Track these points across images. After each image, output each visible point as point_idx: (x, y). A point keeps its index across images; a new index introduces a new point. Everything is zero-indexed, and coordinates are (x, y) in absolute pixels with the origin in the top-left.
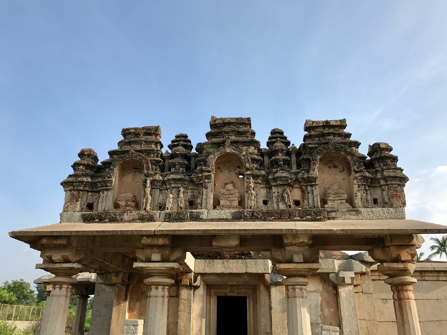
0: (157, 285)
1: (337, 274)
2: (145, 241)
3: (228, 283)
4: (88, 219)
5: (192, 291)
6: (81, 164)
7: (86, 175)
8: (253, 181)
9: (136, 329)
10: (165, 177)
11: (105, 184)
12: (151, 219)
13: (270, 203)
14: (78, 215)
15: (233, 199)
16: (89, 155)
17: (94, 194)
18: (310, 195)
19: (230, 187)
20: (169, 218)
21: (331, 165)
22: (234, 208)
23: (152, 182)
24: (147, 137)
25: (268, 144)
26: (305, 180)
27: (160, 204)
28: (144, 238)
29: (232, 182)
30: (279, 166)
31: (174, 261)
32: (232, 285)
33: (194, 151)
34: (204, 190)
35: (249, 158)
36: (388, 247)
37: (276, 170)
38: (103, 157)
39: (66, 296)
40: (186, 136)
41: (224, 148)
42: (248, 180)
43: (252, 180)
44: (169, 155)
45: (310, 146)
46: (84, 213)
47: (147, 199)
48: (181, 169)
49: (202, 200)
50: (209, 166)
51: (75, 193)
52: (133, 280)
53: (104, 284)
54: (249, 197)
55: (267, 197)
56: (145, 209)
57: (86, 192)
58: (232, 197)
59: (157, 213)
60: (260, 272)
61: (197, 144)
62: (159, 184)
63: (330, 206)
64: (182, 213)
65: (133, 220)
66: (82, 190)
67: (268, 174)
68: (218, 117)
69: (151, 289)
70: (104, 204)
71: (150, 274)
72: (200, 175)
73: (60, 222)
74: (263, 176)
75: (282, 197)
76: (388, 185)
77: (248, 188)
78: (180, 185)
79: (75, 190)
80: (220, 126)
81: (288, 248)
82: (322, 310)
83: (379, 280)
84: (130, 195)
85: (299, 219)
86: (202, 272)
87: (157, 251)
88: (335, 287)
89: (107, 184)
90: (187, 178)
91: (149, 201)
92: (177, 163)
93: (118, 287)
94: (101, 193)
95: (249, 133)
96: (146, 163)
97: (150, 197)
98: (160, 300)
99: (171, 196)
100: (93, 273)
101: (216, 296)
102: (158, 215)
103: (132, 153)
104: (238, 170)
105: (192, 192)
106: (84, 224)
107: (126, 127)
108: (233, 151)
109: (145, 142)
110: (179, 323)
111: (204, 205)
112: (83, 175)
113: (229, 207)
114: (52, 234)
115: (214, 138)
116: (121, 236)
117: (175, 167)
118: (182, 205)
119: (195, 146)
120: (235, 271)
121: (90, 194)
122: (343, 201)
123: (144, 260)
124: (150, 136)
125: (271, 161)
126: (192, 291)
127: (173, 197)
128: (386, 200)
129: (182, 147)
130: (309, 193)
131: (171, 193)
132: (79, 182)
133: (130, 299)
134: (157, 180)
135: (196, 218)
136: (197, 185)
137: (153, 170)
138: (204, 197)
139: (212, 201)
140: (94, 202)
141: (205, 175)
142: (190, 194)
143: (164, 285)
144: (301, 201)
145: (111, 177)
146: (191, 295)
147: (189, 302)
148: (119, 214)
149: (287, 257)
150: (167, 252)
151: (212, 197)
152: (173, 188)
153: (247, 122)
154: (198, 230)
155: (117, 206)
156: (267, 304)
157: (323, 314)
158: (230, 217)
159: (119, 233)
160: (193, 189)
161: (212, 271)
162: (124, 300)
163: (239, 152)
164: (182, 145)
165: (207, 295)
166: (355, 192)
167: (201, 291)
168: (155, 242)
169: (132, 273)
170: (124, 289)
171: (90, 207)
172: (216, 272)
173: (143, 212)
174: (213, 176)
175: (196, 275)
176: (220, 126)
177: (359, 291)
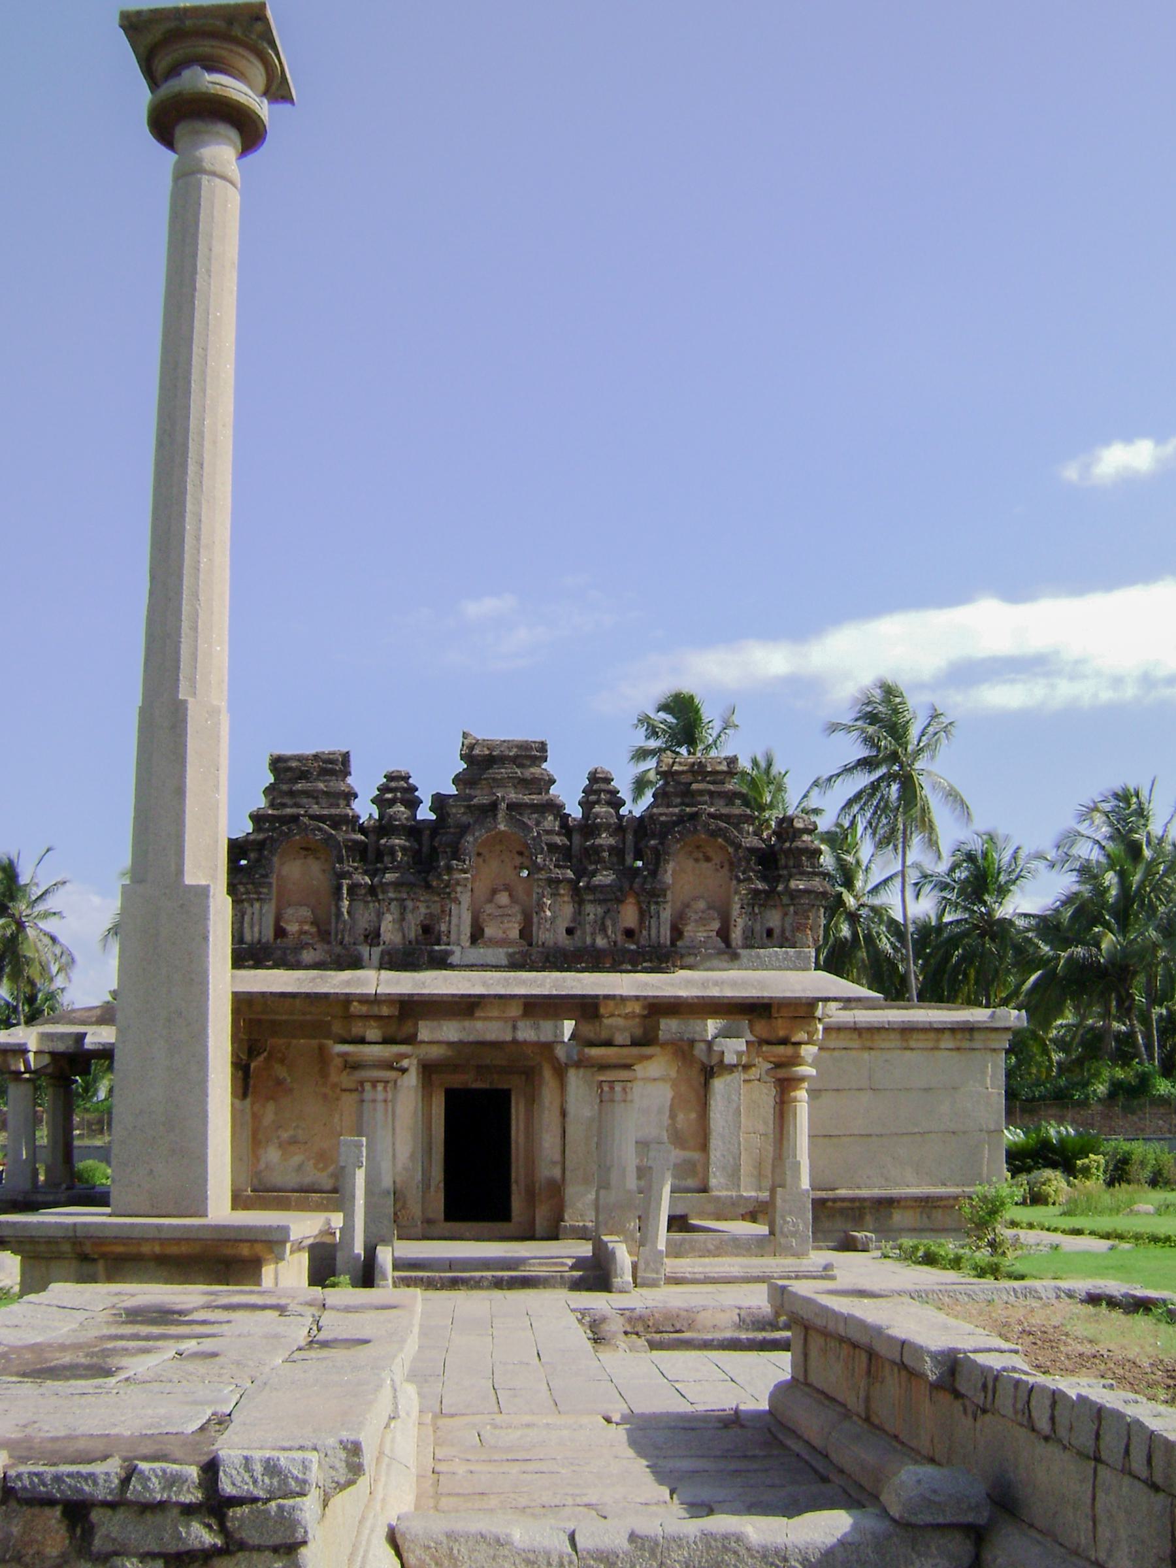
1: (710, 1044)
13: (579, 933)
18: (653, 921)
19: (503, 898)
21: (701, 856)
23: (352, 889)
26: (647, 893)
27: (366, 929)
29: (508, 888)
30: (600, 860)
36: (776, 1018)
37: (593, 867)
45: (663, 818)
55: (574, 920)
56: (341, 943)
59: (365, 950)
60: (543, 1039)
63: (688, 944)
67: (579, 876)
70: (256, 929)
74: (569, 881)
75: (603, 924)
76: (794, 905)
78: (405, 896)
82: (673, 1116)
85: (629, 968)
89: (261, 890)
104: (518, 860)
105: (428, 907)
111: (453, 937)
125: (586, 849)
128: (787, 934)
129: (403, 809)
135: (441, 962)
138: (454, 921)
144: (637, 931)
149: (604, 1035)
152: (392, 900)
153: (534, 753)
156: (557, 1104)
158: (505, 962)
166: (734, 918)
168: (375, 1010)
169: (256, 1040)
173: (338, 950)
177: (753, 1077)
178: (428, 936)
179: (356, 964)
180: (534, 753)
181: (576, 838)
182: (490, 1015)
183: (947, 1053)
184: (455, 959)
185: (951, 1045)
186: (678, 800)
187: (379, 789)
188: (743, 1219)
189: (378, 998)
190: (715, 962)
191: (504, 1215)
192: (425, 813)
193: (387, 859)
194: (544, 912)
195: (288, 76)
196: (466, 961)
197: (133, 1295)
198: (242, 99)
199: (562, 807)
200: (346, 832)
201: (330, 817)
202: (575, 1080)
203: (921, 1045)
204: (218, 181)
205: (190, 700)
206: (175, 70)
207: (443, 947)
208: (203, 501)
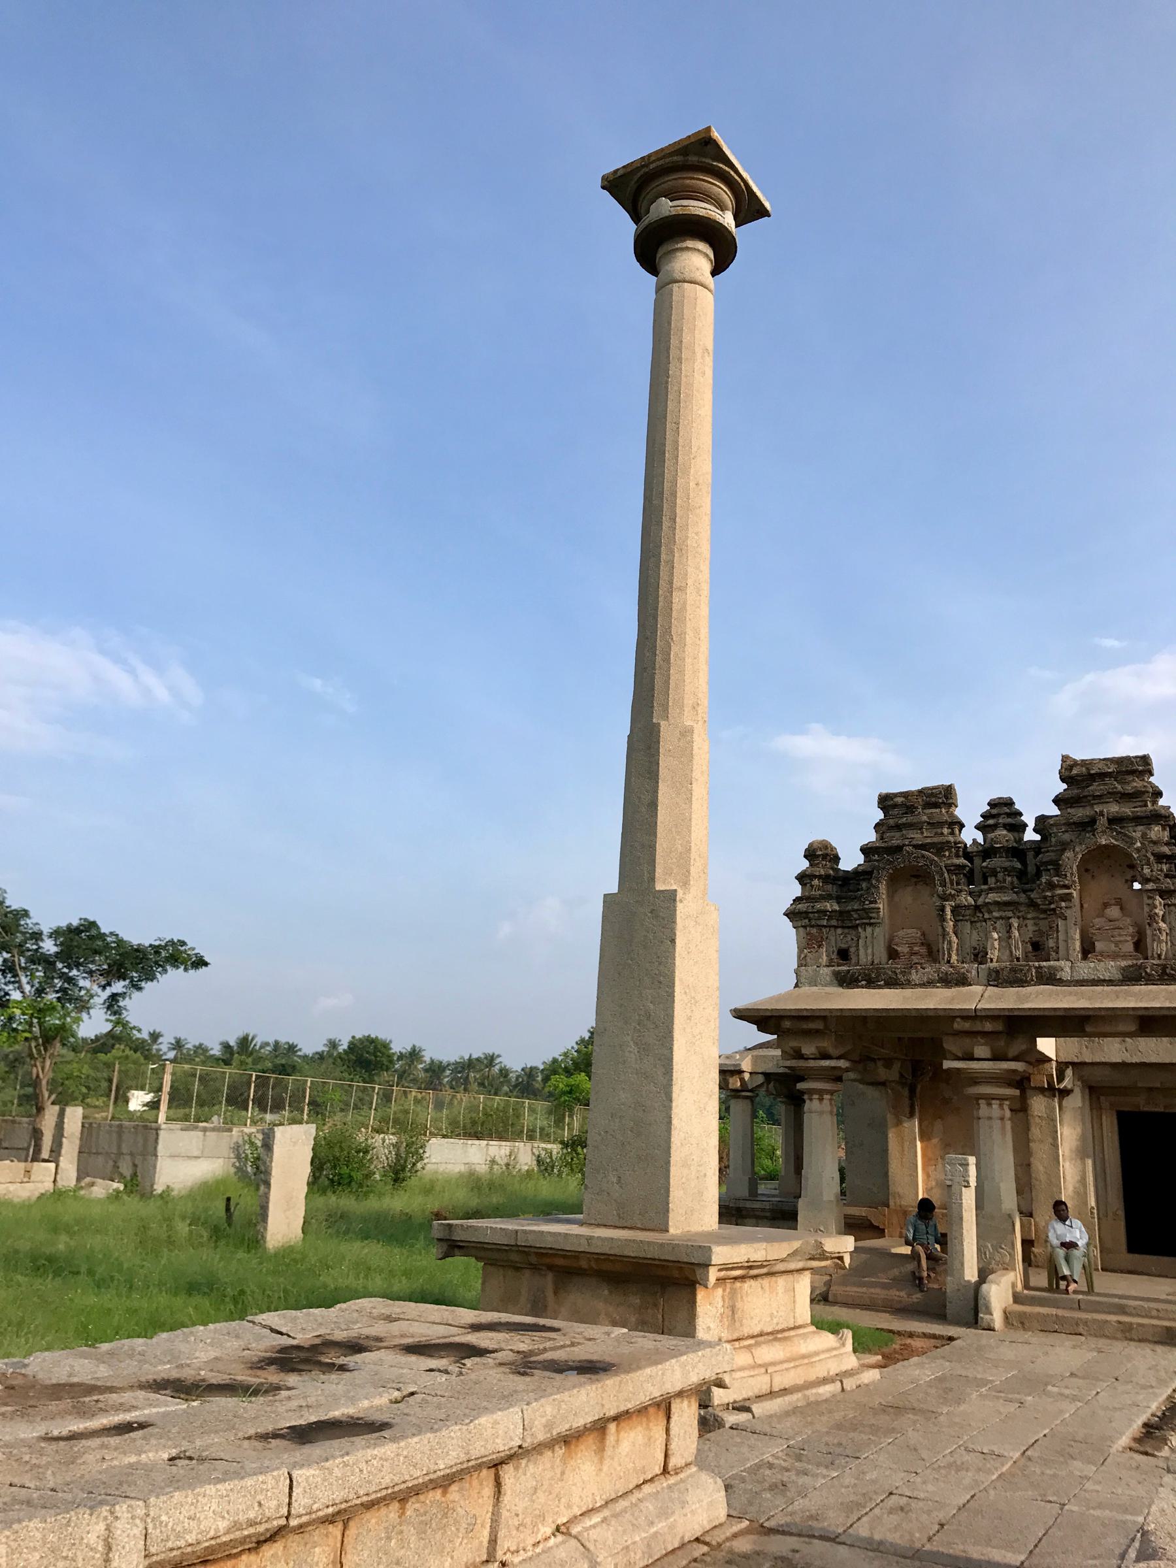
0: (989, 1099)
2: (958, 1025)
3: (1140, 1085)
4: (848, 980)
5: (1056, 1100)
6: (814, 876)
7: (828, 897)
8: (1160, 903)
9: (967, 1171)
10: (979, 896)
11: (867, 913)
12: (962, 981)
14: (826, 972)
15: (1122, 939)
16: (825, 857)
17: (846, 931)
19: (1114, 912)
20: (997, 979)
22: (1124, 957)
24: (931, 811)
28: (958, 1020)
29: (1120, 903)
31: (1015, 1059)
32: (1151, 1089)
33: (1030, 835)
34: (1060, 922)
35: (1149, 855)
38: (851, 860)
39: (831, 1112)
40: (1009, 803)
41: (1094, 835)
42: (1150, 902)
43: (1158, 900)
44: (981, 848)
46: (837, 969)
47: (950, 943)
48: (1009, 879)
49: (1057, 942)
50: (1066, 875)
51: (814, 931)
52: (922, 1075)
53: (861, 1081)
54: (1154, 935)
56: (949, 962)
57: (832, 929)
58: (1120, 935)
59: (972, 969)
61: (1036, 818)
62: (968, 912)
64: (1022, 970)
65: (929, 984)
66: (825, 927)
68: (1078, 756)
70: (870, 951)
71: (975, 1079)
72: (1049, 894)
73: (796, 986)
77: (1152, 917)
78: (1010, 914)
79: (812, 926)
80: (1083, 781)
84: (914, 933)
86: (1076, 1060)
87: (982, 1041)
90: (1023, 898)
91: (955, 946)
92: (998, 869)
93: (892, 1089)
94: (860, 930)
95: (1147, 795)
96: (938, 873)
97: (954, 939)
98: (997, 1124)
99: (995, 935)
101: (1115, 1114)
102: (974, 972)
103: (908, 852)
104: (1129, 874)
106: (841, 990)
107: (885, 791)
108: (1113, 841)
109: (929, 823)
110: (1033, 1167)
112: (823, 898)
113: (1115, 956)
114: (801, 1014)
115: (1071, 807)
117: (996, 876)
118: (1019, 953)
119: (1031, 824)
120: (1154, 1059)
121: (839, 931)
123: (960, 1055)
124: (936, 808)
126: (1056, 1100)
127: (999, 937)
129: (1005, 832)
131: (995, 929)
132: (819, 912)
133: (920, 1111)
134: (965, 906)
135: (1050, 979)
136: (1045, 911)
137: (952, 884)
138: (1061, 936)
139: (1078, 944)
140: (849, 947)
141: (1059, 895)
142: (1031, 928)
143: (1001, 1099)
145: (876, 902)
146: (1055, 1108)
147: (1051, 1123)
148: (902, 972)
150: (1002, 1043)
151: (1077, 936)
152: (997, 918)
154: (1055, 1009)
155: (893, 954)
159: (914, 1014)
160: (1037, 918)
161: (1098, 1059)
162: (908, 1115)
163: (1127, 842)
164: (1005, 826)
165: (1091, 1109)
167: (1076, 1100)
168: (978, 1027)
170: (906, 1092)
171: (844, 955)
172: (1107, 1060)
173: (944, 968)
174: (1075, 894)
175: (1062, 1067)
176: (1083, 781)
178: (1039, 953)
189: (978, 1014)
193: (991, 880)
194: (1157, 923)
195: (755, 189)
198: (702, 213)
200: (949, 857)
201: (933, 845)
204: (686, 284)
205: (662, 723)
208: (676, 550)
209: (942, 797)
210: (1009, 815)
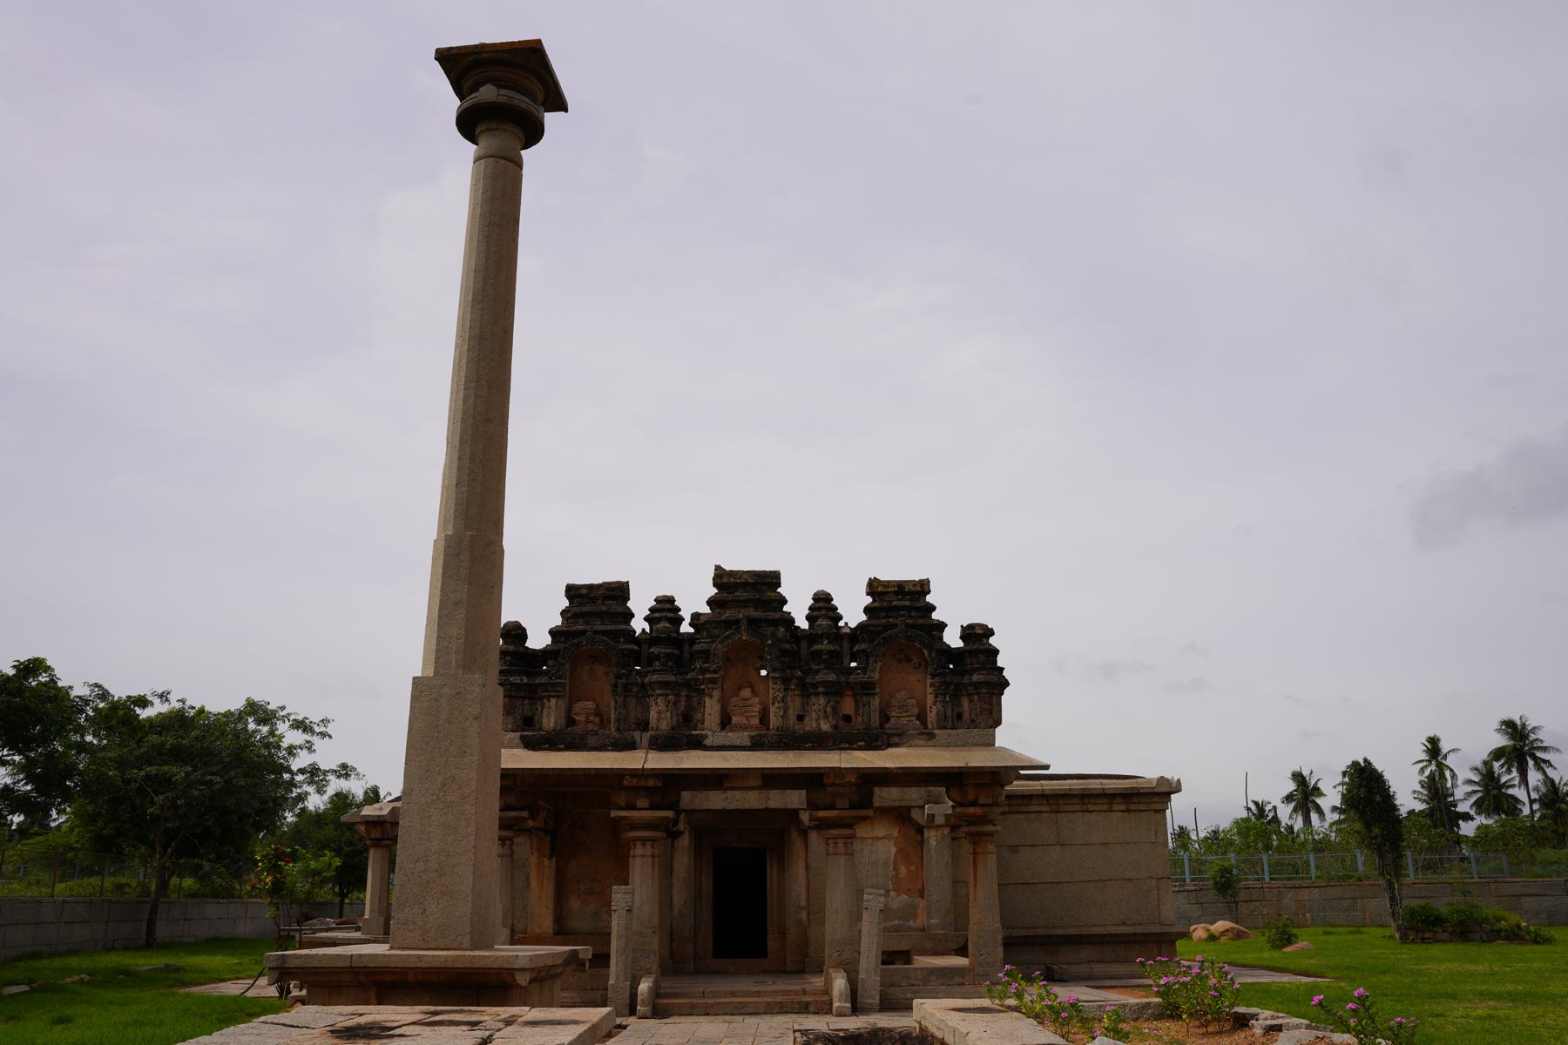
10: (645, 676)
13: (807, 719)
25: (808, 618)
49: (704, 716)
59: (637, 735)
69: (635, 845)
74: (799, 679)
78: (669, 692)
81: (828, 789)
83: (1009, 812)
88: (920, 830)
100: (881, 991)
113: (745, 728)
116: (844, 1039)
119: (688, 620)
121: (526, 702)
122: (912, 718)
123: (623, 805)
130: (864, 706)
135: (697, 744)
144: (854, 717)
152: (659, 695)
153: (772, 579)
157: (897, 876)
168: (643, 783)
179: (630, 746)
180: (772, 579)
181: (804, 645)
182: (734, 785)
183: (1120, 814)
184: (708, 742)
185: (1123, 807)
186: (884, 614)
187: (649, 610)
188: (956, 955)
190: (916, 741)
191: (759, 951)
192: (686, 628)
196: (717, 743)
197: (361, 1015)
198: (523, 105)
199: (793, 620)
202: (813, 836)
203: (1098, 808)
206: (475, 89)
207: (699, 732)
209: (618, 592)
210: (617, 615)
